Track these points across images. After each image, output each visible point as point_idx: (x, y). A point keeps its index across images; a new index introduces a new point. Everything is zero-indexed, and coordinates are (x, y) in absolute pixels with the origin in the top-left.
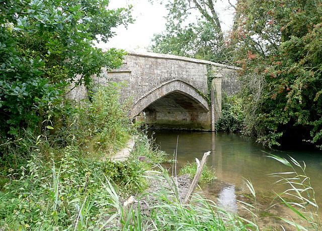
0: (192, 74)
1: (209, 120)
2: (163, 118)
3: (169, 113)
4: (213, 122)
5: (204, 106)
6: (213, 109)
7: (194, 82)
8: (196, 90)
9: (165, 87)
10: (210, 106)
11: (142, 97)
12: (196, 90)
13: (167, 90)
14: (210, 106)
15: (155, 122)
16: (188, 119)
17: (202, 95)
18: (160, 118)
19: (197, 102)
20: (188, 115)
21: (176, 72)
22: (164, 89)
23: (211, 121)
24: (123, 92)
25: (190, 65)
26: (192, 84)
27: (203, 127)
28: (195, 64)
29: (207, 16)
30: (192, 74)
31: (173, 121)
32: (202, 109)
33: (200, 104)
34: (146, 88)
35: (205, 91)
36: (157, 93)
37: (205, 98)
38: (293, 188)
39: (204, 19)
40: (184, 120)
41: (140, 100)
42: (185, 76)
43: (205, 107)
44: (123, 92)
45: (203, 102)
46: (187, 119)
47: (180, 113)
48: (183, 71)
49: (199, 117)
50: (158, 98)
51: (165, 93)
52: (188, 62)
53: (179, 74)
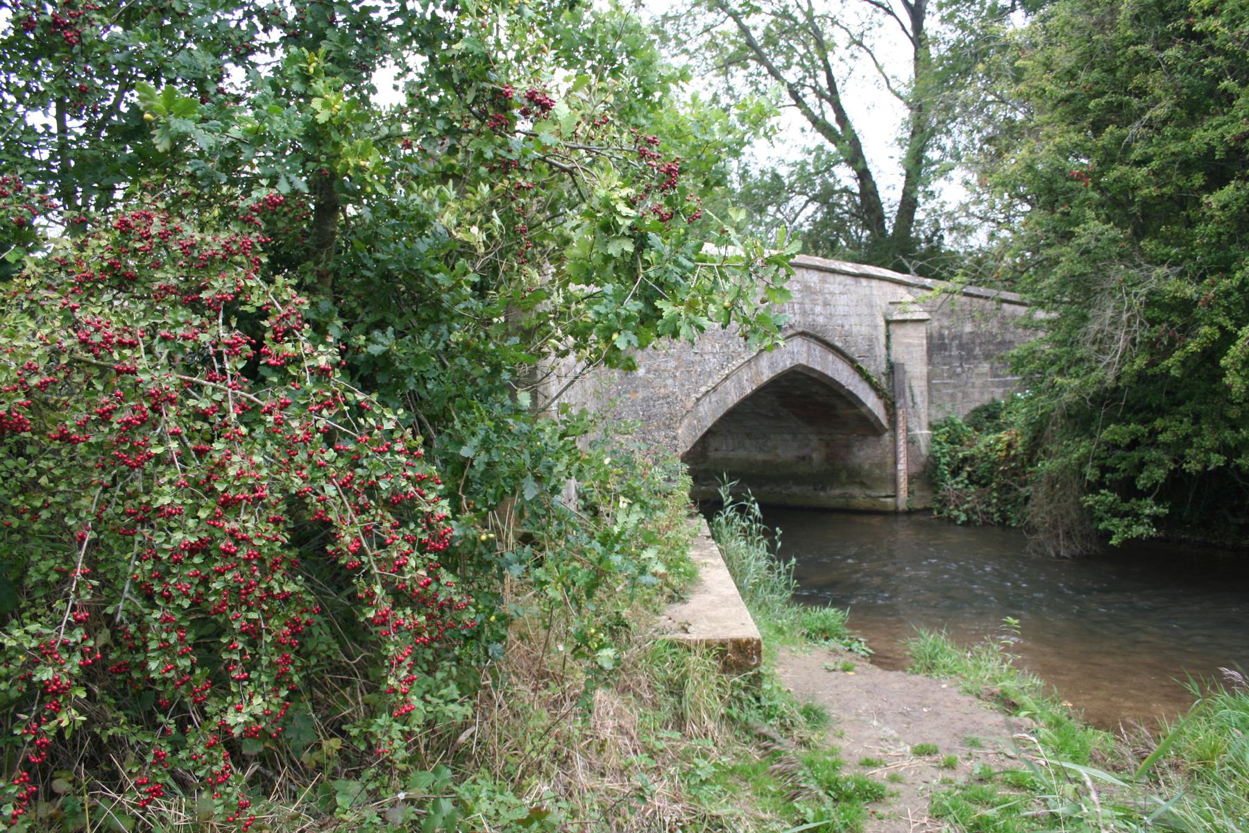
0: (841, 310)
1: (890, 460)
2: (731, 455)
3: (749, 435)
4: (902, 466)
5: (873, 414)
6: (901, 424)
7: (846, 336)
8: (851, 361)
9: (766, 355)
10: (891, 408)
11: (703, 389)
12: (851, 361)
13: (772, 365)
14: (891, 408)
15: (702, 467)
16: (814, 456)
17: (867, 379)
18: (719, 455)
19: (852, 401)
20: (814, 438)
21: (796, 306)
22: (764, 362)
23: (896, 463)
24: (651, 376)
25: (835, 284)
26: (839, 344)
27: (869, 483)
28: (849, 280)
29: (819, 124)
30: (841, 310)
31: (765, 462)
32: (869, 427)
33: (863, 410)
34: (713, 362)
35: (876, 367)
36: (745, 375)
37: (875, 388)
38: (1094, 780)
39: (820, 139)
40: (803, 458)
41: (698, 400)
42: (821, 320)
43: (877, 418)
44: (651, 376)
45: (872, 402)
46: (811, 458)
47: (788, 437)
48: (815, 304)
49: (855, 450)
50: (749, 391)
51: (767, 375)
52: (827, 274)
53: (804, 313)
